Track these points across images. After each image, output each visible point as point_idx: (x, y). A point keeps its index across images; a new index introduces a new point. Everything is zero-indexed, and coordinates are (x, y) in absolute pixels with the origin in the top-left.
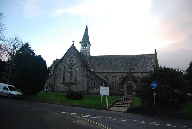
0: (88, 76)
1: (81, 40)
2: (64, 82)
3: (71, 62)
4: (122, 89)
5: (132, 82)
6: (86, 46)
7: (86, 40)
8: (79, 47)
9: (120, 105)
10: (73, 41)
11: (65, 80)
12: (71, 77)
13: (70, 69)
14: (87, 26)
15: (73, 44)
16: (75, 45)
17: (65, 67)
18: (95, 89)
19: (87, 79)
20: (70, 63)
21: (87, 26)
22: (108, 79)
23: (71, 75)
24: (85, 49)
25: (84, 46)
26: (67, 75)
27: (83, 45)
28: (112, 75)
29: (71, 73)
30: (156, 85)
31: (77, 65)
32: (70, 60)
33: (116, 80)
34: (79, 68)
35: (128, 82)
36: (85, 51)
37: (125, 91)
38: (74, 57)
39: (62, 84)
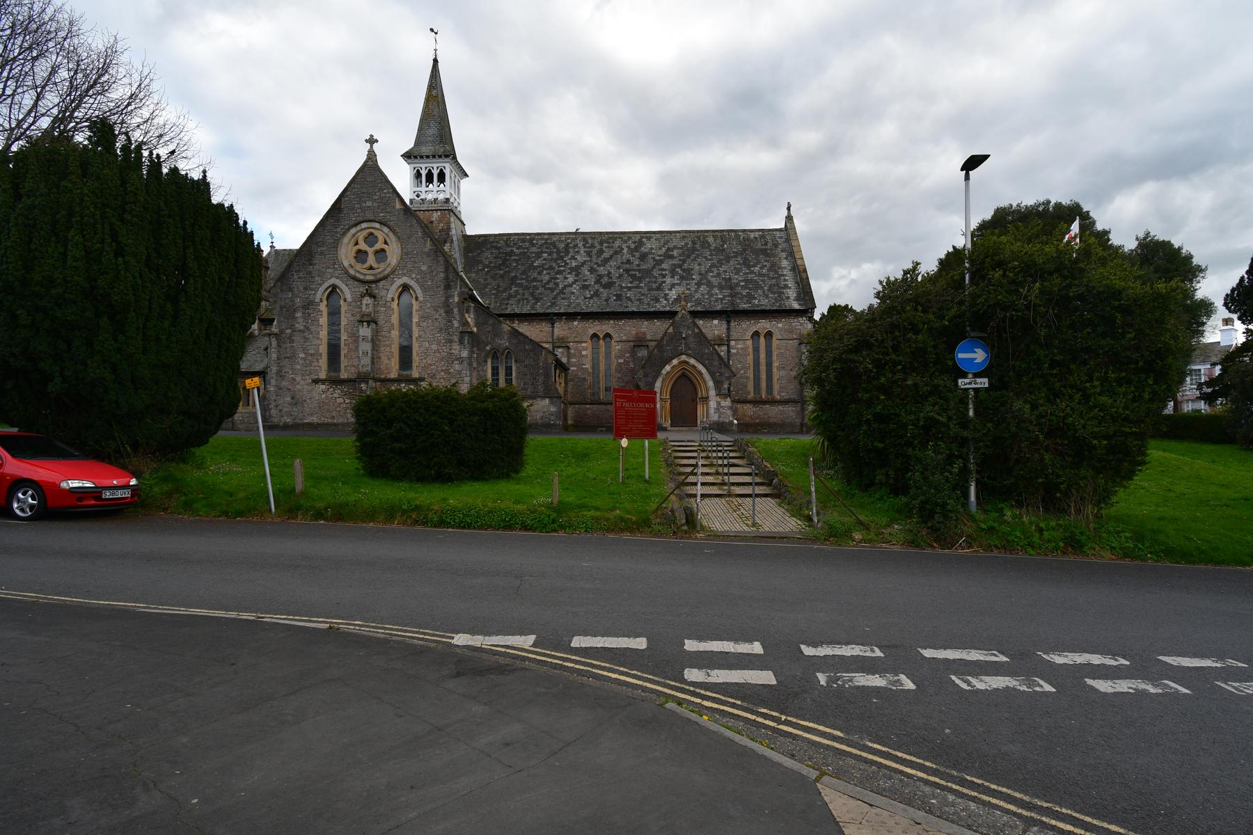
0: (473, 340)
1: (409, 144)
2: (338, 370)
3: (371, 260)
5: (692, 361)
7: (435, 142)
8: (401, 177)
11: (344, 362)
12: (375, 342)
13: (367, 300)
14: (435, 61)
15: (372, 156)
16: (382, 164)
17: (334, 287)
19: (465, 354)
20: (359, 266)
21: (435, 61)
23: (376, 334)
24: (433, 192)
26: (355, 337)
27: (424, 173)
28: (591, 332)
29: (376, 323)
30: (979, 356)
31: (405, 280)
32: (359, 251)
33: (608, 354)
34: (419, 291)
35: (675, 362)
36: (434, 206)
37: (662, 407)
38: (386, 229)
39: (323, 381)
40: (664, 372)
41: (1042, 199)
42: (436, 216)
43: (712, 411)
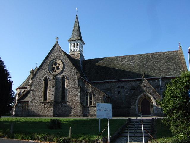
1: (69, 37)
4: (134, 106)
6: (77, 45)
8: (69, 49)
9: (133, 130)
10: (57, 39)
15: (57, 42)
18: (92, 108)
22: (111, 91)
25: (74, 45)
28: (118, 86)
40: (138, 98)
41: (11, 76)
42: (76, 56)
43: (155, 110)
